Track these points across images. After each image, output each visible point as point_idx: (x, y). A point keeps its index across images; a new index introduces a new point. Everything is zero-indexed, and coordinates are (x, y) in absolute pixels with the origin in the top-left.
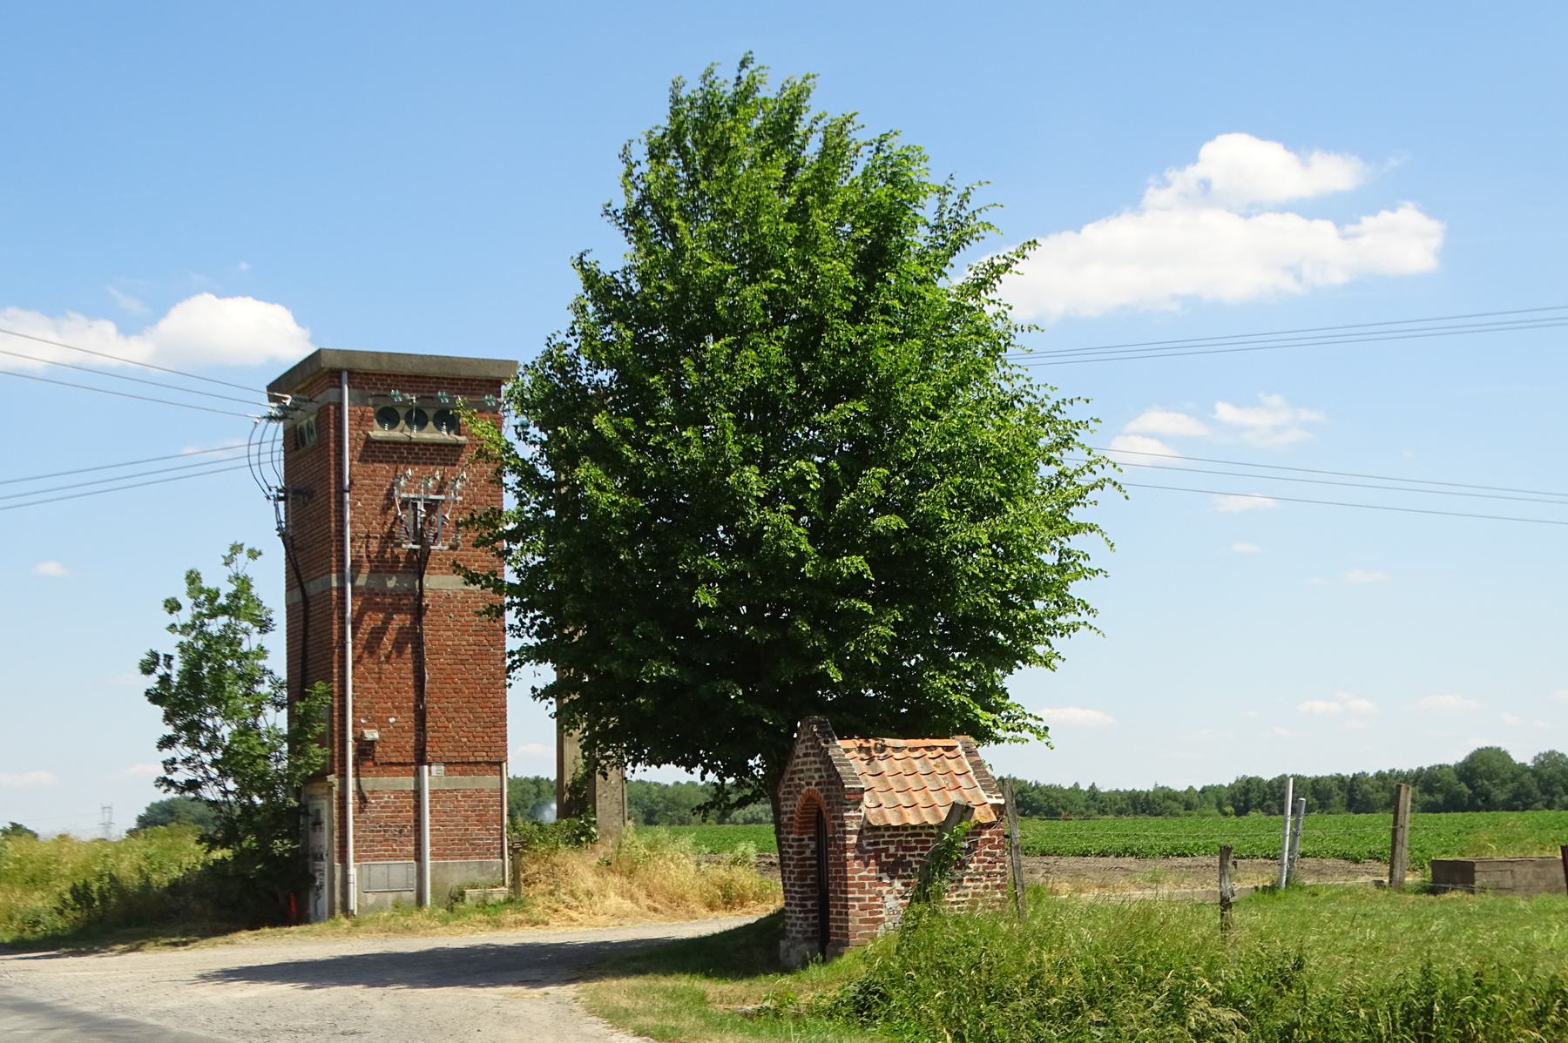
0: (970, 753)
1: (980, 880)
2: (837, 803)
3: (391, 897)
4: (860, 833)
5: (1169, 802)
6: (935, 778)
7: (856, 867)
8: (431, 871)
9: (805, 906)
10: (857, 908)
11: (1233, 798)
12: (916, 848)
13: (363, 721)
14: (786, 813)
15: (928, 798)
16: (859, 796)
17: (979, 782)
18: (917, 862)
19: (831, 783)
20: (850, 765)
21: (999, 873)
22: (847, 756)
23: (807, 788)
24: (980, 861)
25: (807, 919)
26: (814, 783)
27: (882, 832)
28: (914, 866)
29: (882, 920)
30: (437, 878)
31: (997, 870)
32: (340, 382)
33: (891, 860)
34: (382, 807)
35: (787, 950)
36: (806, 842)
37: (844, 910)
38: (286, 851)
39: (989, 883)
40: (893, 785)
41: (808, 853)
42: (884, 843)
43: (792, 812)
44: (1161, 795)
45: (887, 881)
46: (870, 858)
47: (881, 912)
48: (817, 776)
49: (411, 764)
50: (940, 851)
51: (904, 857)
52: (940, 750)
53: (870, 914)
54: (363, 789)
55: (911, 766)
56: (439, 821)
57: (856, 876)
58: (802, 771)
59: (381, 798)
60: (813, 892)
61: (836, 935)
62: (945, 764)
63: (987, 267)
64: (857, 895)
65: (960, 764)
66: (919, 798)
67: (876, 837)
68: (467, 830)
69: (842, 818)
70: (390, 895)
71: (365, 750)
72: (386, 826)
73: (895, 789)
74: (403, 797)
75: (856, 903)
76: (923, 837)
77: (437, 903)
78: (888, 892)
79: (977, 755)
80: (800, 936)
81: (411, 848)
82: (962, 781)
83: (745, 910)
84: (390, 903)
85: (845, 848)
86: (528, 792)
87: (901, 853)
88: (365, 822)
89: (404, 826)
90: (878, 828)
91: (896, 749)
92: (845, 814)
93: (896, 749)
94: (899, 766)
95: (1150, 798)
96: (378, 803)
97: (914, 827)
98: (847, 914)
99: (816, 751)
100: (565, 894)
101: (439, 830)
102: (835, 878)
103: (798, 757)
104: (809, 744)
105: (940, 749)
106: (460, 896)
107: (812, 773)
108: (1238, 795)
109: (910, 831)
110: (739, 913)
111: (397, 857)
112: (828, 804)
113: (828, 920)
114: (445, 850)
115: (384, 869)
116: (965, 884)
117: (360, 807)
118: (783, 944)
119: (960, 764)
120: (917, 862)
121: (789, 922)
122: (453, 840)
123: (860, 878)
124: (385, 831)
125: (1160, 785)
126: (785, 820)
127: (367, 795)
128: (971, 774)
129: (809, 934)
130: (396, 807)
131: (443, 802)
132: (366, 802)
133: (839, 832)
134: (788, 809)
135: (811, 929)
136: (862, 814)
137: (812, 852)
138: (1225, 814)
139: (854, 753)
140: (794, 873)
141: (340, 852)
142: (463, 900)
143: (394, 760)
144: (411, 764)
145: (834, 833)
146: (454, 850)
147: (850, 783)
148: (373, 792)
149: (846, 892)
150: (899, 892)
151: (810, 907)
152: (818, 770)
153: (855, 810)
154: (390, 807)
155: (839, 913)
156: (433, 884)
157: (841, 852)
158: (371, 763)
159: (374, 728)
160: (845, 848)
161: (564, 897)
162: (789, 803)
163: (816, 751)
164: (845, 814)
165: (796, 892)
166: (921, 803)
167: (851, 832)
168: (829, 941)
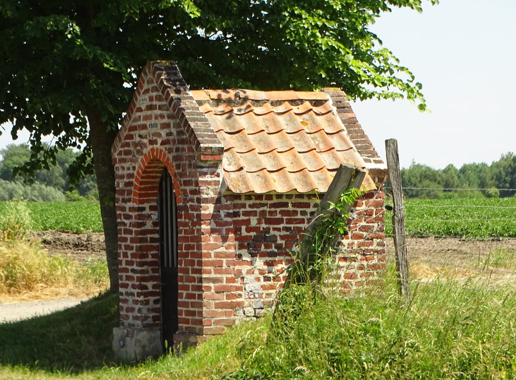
0: (342, 108)
1: (354, 260)
2: (190, 166)
4: (218, 201)
5: (426, 182)
6: (302, 138)
7: (212, 242)
9: (146, 287)
10: (213, 291)
11: (499, 178)
12: (280, 221)
14: (122, 177)
15: (296, 161)
16: (217, 158)
18: (282, 238)
19: (182, 142)
20: (206, 120)
21: (377, 252)
22: (202, 109)
23: (150, 147)
24: (356, 237)
25: (147, 302)
26: (159, 141)
27: (242, 201)
28: (279, 241)
29: (240, 305)
31: (374, 247)
33: (253, 234)
35: (123, 339)
36: (147, 212)
37: (197, 293)
39: (365, 263)
40: (254, 145)
41: (149, 225)
42: (246, 214)
43: (131, 176)
44: (418, 175)
45: (247, 258)
46: (228, 231)
47: (240, 295)
48: (163, 133)
50: (324, 224)
51: (267, 230)
52: (308, 105)
53: (228, 297)
55: (275, 122)
58: (144, 127)
60: (154, 271)
61: (187, 321)
62: (314, 122)
64: (213, 275)
66: (285, 160)
67: (235, 206)
69: (197, 184)
73: (257, 151)
75: (212, 285)
76: (290, 208)
78: (249, 272)
79: (351, 111)
80: (139, 322)
82: (334, 141)
83: (33, 293)
85: (200, 219)
87: (264, 226)
90: (238, 196)
93: (257, 102)
94: (261, 123)
95: (406, 177)
97: (279, 196)
98: (200, 297)
99: (164, 103)
102: (186, 255)
103: (140, 110)
104: (154, 94)
105: (307, 104)
107: (158, 130)
108: (503, 174)
109: (275, 200)
110: (25, 297)
112: (178, 166)
113: (176, 303)
118: (117, 332)
119: (331, 122)
120: (282, 238)
121: (125, 306)
123: (217, 255)
125: (416, 164)
126: (121, 185)
128: (345, 133)
129: (150, 321)
133: (192, 200)
134: (126, 172)
135: (151, 315)
136: (220, 179)
137: (155, 224)
138: (489, 196)
139: (207, 107)
140: (131, 248)
145: (185, 201)
147: (208, 142)
149: (200, 272)
150: (261, 272)
151: (151, 289)
152: (166, 126)
153: (212, 173)
155: (191, 296)
157: (194, 224)
160: (200, 219)
162: (126, 165)
163: (164, 103)
164: (200, 179)
165: (133, 271)
166: (289, 168)
167: (206, 201)
168: (177, 328)
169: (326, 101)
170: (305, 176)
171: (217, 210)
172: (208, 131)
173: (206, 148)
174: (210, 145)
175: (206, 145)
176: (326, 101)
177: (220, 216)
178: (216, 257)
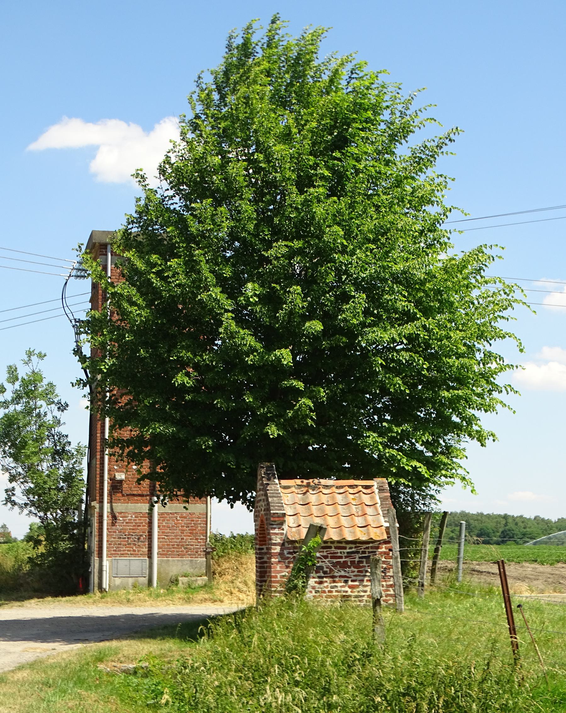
3: (131, 581)
4: (283, 545)
7: (278, 569)
8: (158, 564)
13: (116, 467)
16: (281, 519)
17: (382, 511)
20: (281, 497)
30: (162, 569)
32: (106, 252)
34: (127, 523)
38: (66, 549)
46: (289, 563)
49: (147, 495)
52: (360, 488)
54: (115, 511)
55: (333, 498)
56: (163, 532)
57: (279, 575)
59: (127, 517)
62: (360, 497)
63: (422, 148)
65: (372, 498)
68: (182, 539)
70: (130, 579)
71: (116, 486)
72: (129, 535)
74: (141, 517)
77: (161, 584)
81: (146, 550)
84: (130, 584)
86: (500, 523)
88: (115, 532)
89: (141, 535)
91: (326, 487)
92: (271, 531)
93: (326, 487)
96: (124, 520)
100: (240, 582)
101: (163, 538)
106: (175, 582)
111: (136, 555)
114: (168, 551)
115: (127, 563)
116: (365, 583)
117: (112, 523)
119: (372, 498)
122: (174, 545)
124: (128, 538)
127: (117, 514)
130: (136, 523)
131: (167, 520)
132: (116, 519)
141: (99, 551)
142: (177, 585)
143: (135, 493)
144: (147, 495)
146: (174, 551)
148: (120, 513)
153: (279, 528)
154: (132, 523)
156: (159, 573)
158: (120, 495)
159: (123, 472)
161: (240, 585)
164: (271, 531)
167: (275, 544)
169: (373, 486)
170: (341, 530)
171: (282, 550)
172: (279, 503)
173: (274, 514)
174: (277, 512)
175: (274, 512)
176: (373, 486)
177: (284, 553)
178: (281, 578)
